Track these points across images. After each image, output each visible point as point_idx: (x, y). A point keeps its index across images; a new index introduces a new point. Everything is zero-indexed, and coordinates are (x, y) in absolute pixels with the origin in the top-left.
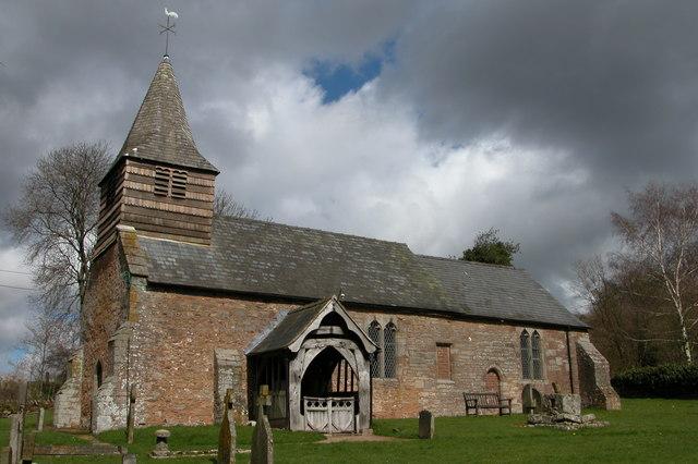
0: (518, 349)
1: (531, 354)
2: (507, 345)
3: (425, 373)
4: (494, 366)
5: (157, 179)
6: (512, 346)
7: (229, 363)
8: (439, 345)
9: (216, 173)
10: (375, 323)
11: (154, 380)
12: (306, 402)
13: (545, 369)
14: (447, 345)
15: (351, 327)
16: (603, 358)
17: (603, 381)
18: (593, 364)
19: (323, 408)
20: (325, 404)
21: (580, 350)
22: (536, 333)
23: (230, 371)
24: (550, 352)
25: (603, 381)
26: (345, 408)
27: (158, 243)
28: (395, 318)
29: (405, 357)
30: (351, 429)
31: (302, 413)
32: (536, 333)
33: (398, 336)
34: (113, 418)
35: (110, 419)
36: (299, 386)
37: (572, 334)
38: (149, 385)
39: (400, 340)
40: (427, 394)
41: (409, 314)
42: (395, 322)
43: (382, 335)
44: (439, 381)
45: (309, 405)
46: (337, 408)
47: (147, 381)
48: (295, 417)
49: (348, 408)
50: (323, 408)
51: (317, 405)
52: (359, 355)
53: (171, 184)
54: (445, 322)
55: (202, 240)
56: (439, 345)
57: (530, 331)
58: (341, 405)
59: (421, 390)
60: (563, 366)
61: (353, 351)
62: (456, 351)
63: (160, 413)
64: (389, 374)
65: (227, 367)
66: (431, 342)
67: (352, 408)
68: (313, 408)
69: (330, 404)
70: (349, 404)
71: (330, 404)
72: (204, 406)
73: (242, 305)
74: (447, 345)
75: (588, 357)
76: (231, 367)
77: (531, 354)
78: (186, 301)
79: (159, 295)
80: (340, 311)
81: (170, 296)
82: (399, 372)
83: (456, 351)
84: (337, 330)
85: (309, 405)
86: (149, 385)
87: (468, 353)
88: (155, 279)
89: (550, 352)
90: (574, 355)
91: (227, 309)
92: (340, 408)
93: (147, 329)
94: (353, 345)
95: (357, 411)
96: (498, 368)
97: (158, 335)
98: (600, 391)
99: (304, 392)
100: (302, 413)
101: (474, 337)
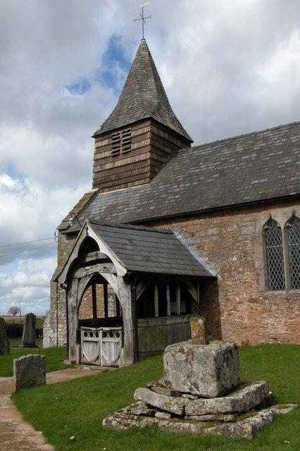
10: (271, 222)
31: (78, 341)
46: (108, 339)
53: (122, 143)
55: (142, 181)
71: (100, 334)
85: (86, 335)
100: (78, 341)
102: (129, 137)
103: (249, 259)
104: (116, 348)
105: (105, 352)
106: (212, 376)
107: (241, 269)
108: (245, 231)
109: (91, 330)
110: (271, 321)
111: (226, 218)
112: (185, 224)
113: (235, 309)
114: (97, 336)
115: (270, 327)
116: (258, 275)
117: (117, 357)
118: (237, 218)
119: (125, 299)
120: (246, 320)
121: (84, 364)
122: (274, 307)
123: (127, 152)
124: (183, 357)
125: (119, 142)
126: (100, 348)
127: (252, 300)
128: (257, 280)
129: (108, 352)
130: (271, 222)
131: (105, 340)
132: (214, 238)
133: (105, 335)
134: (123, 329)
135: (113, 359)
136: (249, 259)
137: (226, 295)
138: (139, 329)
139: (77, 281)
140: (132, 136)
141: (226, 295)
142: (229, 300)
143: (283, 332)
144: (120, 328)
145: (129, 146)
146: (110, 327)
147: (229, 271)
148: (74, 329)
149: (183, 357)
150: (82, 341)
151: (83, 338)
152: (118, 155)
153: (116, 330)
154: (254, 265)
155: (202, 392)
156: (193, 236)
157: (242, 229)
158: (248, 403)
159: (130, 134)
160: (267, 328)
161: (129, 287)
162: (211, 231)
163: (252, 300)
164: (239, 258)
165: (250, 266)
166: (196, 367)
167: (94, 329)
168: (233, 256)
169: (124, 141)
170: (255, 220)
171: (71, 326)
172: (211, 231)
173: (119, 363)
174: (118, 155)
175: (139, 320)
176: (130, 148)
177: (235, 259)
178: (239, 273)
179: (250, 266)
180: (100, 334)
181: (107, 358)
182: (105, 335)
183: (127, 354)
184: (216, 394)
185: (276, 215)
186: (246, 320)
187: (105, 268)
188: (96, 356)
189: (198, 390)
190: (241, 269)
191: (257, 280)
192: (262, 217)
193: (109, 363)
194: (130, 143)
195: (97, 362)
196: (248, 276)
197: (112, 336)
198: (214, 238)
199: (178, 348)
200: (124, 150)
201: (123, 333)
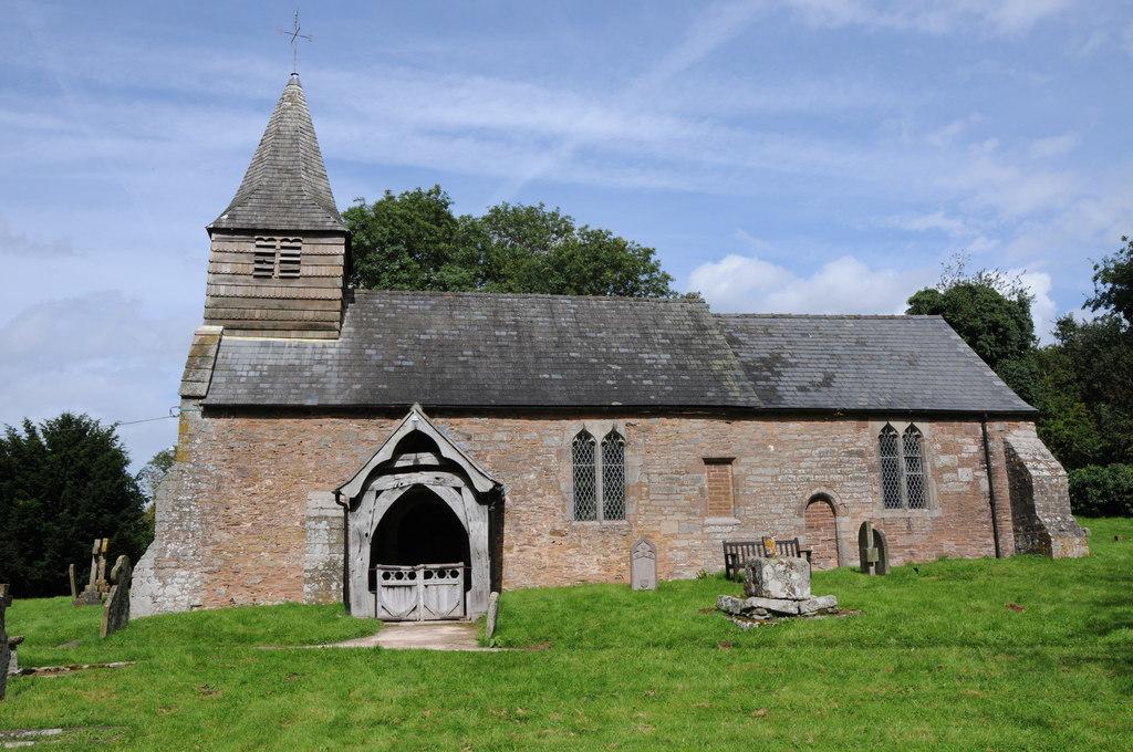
0: (875, 459)
1: (903, 464)
2: (850, 454)
3: (681, 509)
4: (823, 490)
5: (257, 254)
6: (860, 454)
7: (323, 513)
8: (708, 461)
9: (210, 231)
10: (584, 435)
11: (215, 543)
12: (380, 573)
13: (933, 490)
14: (728, 461)
15: (447, 452)
16: (1057, 464)
17: (1052, 507)
18: (1030, 476)
19: (409, 582)
20: (412, 576)
21: (1010, 453)
22: (913, 428)
23: (323, 525)
24: (945, 460)
25: (1052, 507)
26: (448, 580)
27: (252, 345)
28: (620, 425)
29: (640, 485)
30: (458, 612)
31: (373, 586)
32: (913, 428)
33: (627, 453)
34: (154, 598)
35: (149, 601)
36: (367, 550)
37: (995, 427)
38: (208, 550)
39: (632, 458)
40: (684, 543)
41: (647, 416)
42: (621, 430)
43: (599, 452)
44: (709, 520)
45: (386, 576)
46: (435, 580)
47: (205, 544)
48: (359, 597)
49: (454, 580)
50: (409, 582)
51: (399, 576)
52: (467, 494)
53: (278, 258)
54: (720, 425)
55: (324, 334)
56: (708, 461)
57: (900, 427)
58: (442, 574)
59: (674, 536)
60: (974, 483)
61: (458, 490)
62: (743, 469)
63: (223, 590)
64: (615, 511)
65: (320, 519)
66: (693, 458)
67: (460, 579)
68: (393, 581)
69: (420, 574)
70: (455, 574)
71: (420, 574)
72: (292, 576)
73: (352, 425)
74: (728, 461)
75: (1022, 465)
76: (326, 518)
77: (903, 464)
78: (263, 426)
79: (223, 422)
80: (425, 428)
81: (238, 422)
82: (630, 510)
83: (743, 469)
84: (427, 458)
85: (386, 576)
86: (208, 550)
87: (769, 471)
88: (212, 400)
89: (945, 460)
90: (999, 462)
91: (328, 432)
92: (439, 581)
93: (206, 472)
94: (458, 481)
95: (467, 586)
96: (829, 492)
97: (221, 479)
98: (1041, 527)
99: (378, 557)
100: (373, 586)
101: (778, 443)
102: (297, 252)
103: (553, 478)
107: (540, 491)
108: (548, 441)
110: (578, 558)
111: (522, 422)
112: (457, 421)
113: (529, 544)
115: (578, 566)
116: (564, 500)
118: (539, 424)
122: (584, 542)
123: (290, 275)
124: (782, 568)
125: (273, 255)
127: (554, 532)
128: (563, 507)
130: (584, 435)
131: (428, 581)
132: (503, 446)
133: (428, 575)
136: (553, 478)
137: (518, 524)
139: (374, 494)
140: (303, 251)
141: (518, 524)
142: (521, 531)
143: (595, 572)
145: (295, 267)
147: (523, 492)
149: (782, 568)
152: (270, 277)
154: (559, 488)
156: (469, 439)
158: (1016, 562)
159: (299, 248)
161: (486, 507)
162: (498, 436)
163: (554, 532)
164: (540, 475)
165: (555, 487)
168: (530, 472)
169: (283, 255)
170: (563, 430)
172: (498, 436)
174: (270, 277)
176: (298, 271)
177: (532, 476)
178: (538, 495)
179: (555, 487)
182: (428, 575)
185: (592, 427)
187: (437, 478)
190: (540, 491)
191: (563, 507)
192: (573, 427)
194: (298, 262)
196: (550, 500)
198: (503, 446)
200: (282, 271)
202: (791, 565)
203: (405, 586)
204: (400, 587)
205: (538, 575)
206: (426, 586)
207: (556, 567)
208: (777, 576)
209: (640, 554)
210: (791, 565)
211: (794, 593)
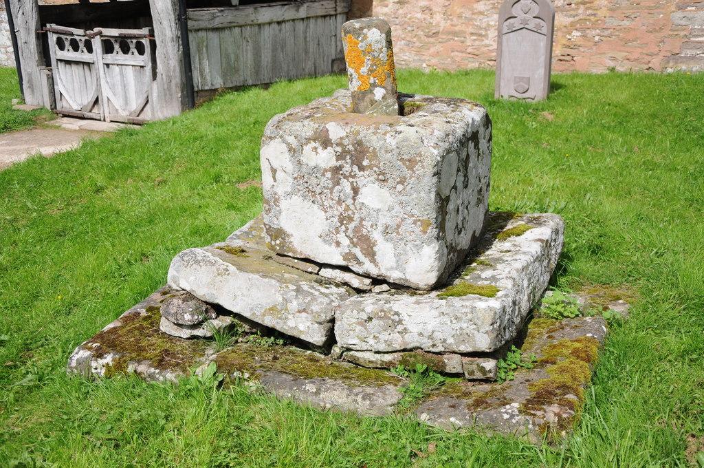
12: (52, 39)
31: (45, 57)
46: (118, 57)
48: (30, 75)
68: (69, 54)
71: (97, 44)
100: (45, 57)
104: (139, 82)
105: (112, 87)
106: (426, 224)
109: (72, 34)
114: (90, 50)
117: (142, 101)
119: (450, 231)
120: (438, 17)
121: (65, 116)
124: (325, 158)
126: (98, 80)
129: (119, 89)
131: (109, 58)
133: (108, 47)
134: (152, 34)
135: (135, 105)
138: (191, 36)
144: (145, 31)
146: (119, 27)
148: (27, 30)
149: (325, 158)
150: (53, 62)
151: (55, 53)
153: (134, 37)
155: (386, 263)
157: (240, 29)
160: (486, 36)
166: (373, 196)
167: (80, 32)
171: (18, 21)
173: (147, 115)
175: (190, 12)
180: (97, 44)
181: (117, 103)
182: (108, 47)
183: (166, 94)
184: (432, 279)
186: (438, 17)
188: (91, 98)
189: (373, 261)
193: (123, 114)
195: (95, 110)
197: (125, 50)
199: (308, 128)
201: (153, 45)
202: (357, 154)
203: (84, 63)
204: (77, 63)
205: (426, 46)
206: (108, 65)
207: (455, 34)
208: (306, 183)
209: (516, 23)
210: (357, 154)
211: (371, 255)
